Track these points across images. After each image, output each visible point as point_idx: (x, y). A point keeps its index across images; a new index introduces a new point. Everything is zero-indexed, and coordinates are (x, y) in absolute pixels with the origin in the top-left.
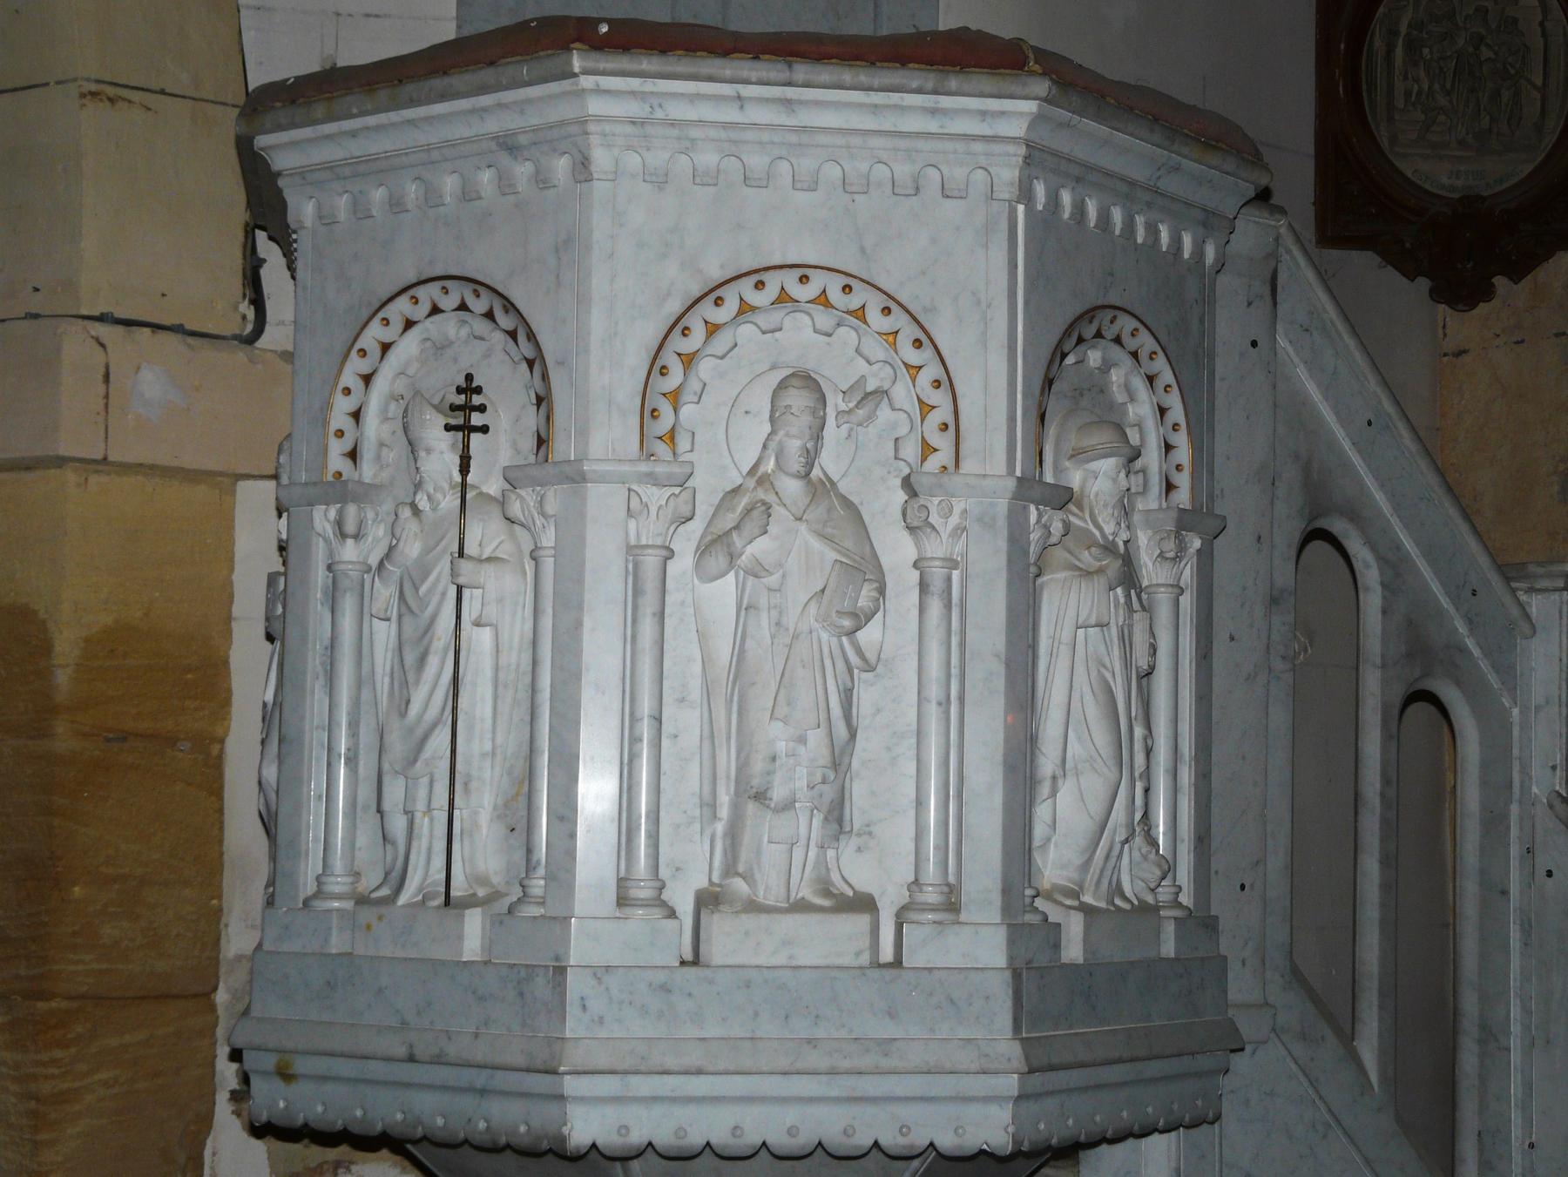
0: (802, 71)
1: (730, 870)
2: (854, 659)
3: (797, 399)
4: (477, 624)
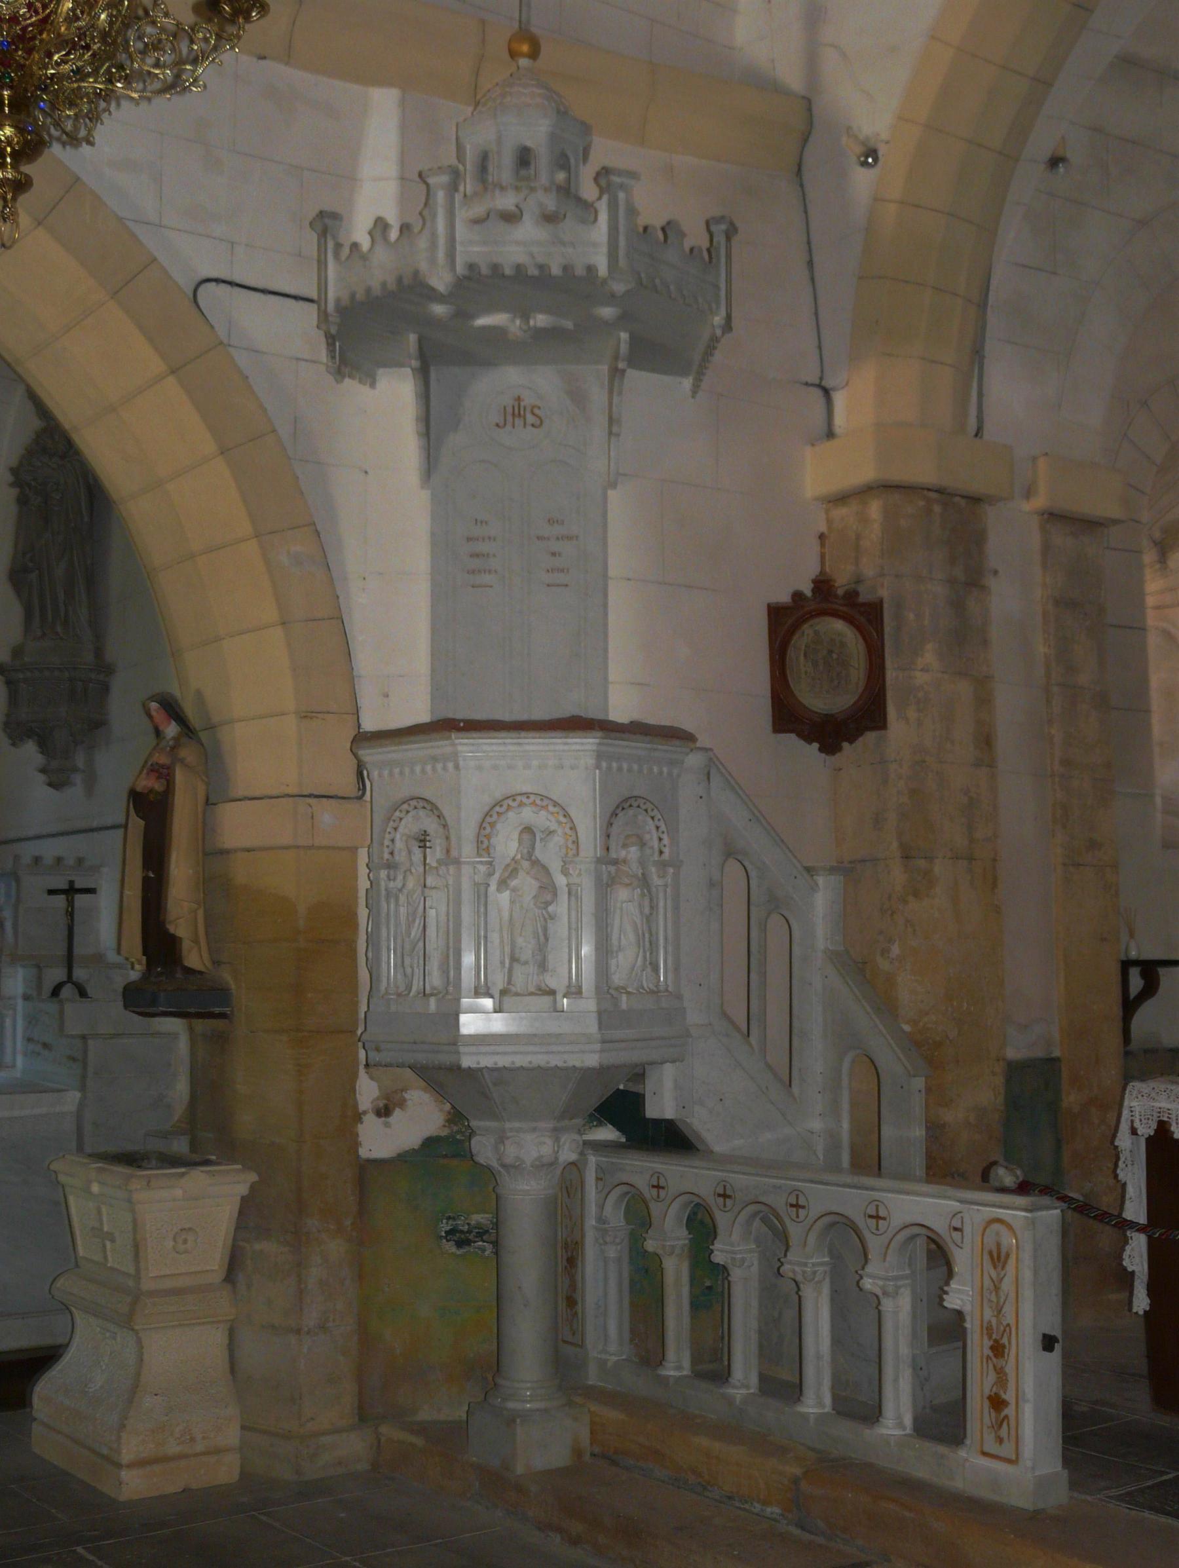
0: (523, 734)
1: (509, 983)
2: (547, 916)
3: (526, 836)
4: (431, 908)
